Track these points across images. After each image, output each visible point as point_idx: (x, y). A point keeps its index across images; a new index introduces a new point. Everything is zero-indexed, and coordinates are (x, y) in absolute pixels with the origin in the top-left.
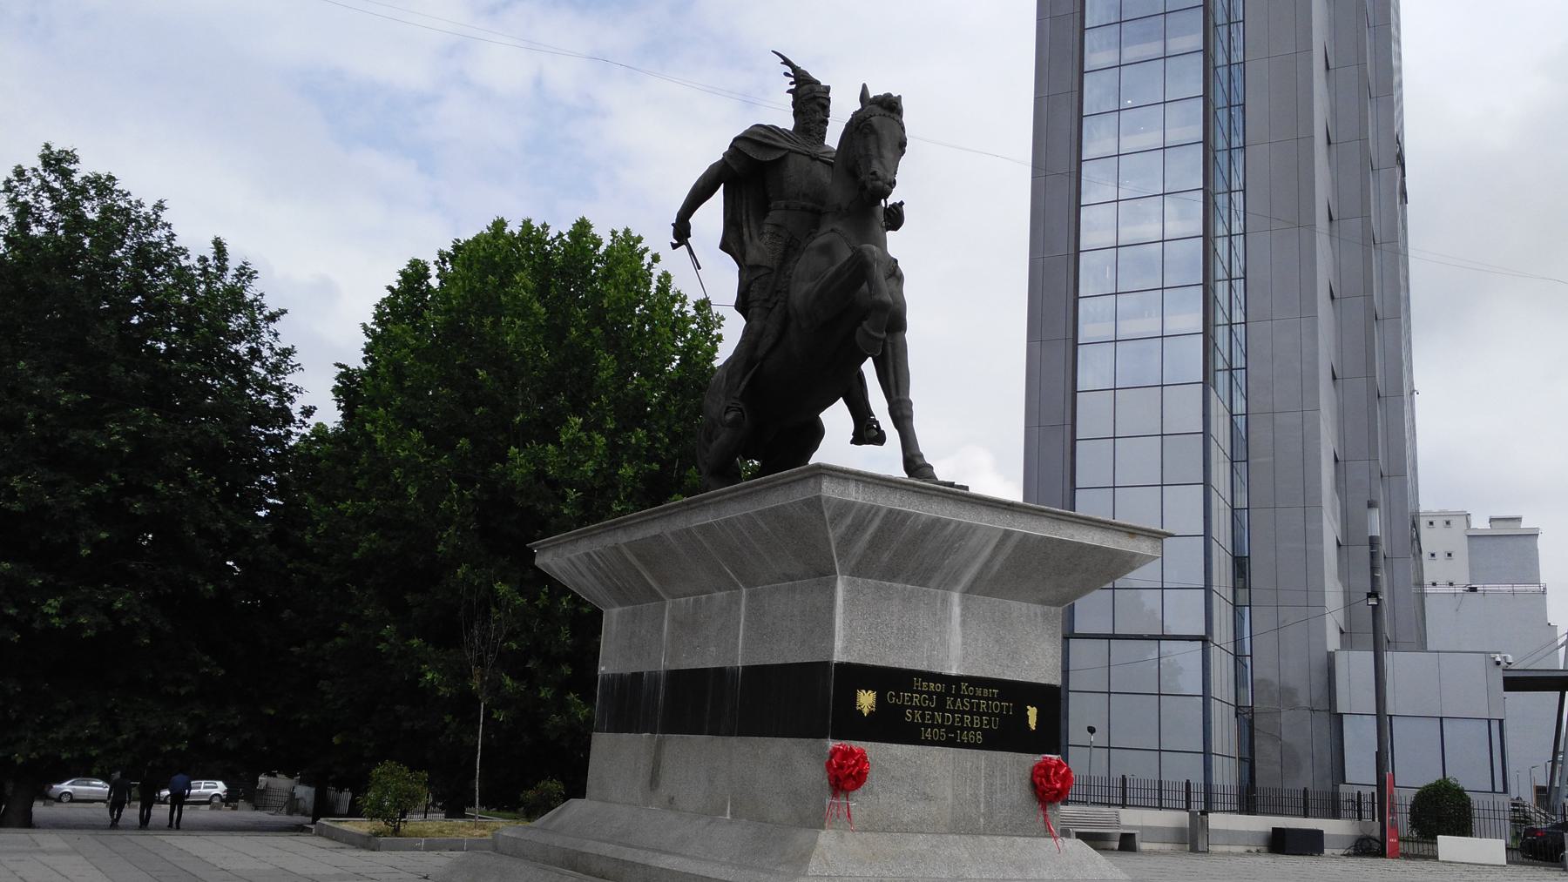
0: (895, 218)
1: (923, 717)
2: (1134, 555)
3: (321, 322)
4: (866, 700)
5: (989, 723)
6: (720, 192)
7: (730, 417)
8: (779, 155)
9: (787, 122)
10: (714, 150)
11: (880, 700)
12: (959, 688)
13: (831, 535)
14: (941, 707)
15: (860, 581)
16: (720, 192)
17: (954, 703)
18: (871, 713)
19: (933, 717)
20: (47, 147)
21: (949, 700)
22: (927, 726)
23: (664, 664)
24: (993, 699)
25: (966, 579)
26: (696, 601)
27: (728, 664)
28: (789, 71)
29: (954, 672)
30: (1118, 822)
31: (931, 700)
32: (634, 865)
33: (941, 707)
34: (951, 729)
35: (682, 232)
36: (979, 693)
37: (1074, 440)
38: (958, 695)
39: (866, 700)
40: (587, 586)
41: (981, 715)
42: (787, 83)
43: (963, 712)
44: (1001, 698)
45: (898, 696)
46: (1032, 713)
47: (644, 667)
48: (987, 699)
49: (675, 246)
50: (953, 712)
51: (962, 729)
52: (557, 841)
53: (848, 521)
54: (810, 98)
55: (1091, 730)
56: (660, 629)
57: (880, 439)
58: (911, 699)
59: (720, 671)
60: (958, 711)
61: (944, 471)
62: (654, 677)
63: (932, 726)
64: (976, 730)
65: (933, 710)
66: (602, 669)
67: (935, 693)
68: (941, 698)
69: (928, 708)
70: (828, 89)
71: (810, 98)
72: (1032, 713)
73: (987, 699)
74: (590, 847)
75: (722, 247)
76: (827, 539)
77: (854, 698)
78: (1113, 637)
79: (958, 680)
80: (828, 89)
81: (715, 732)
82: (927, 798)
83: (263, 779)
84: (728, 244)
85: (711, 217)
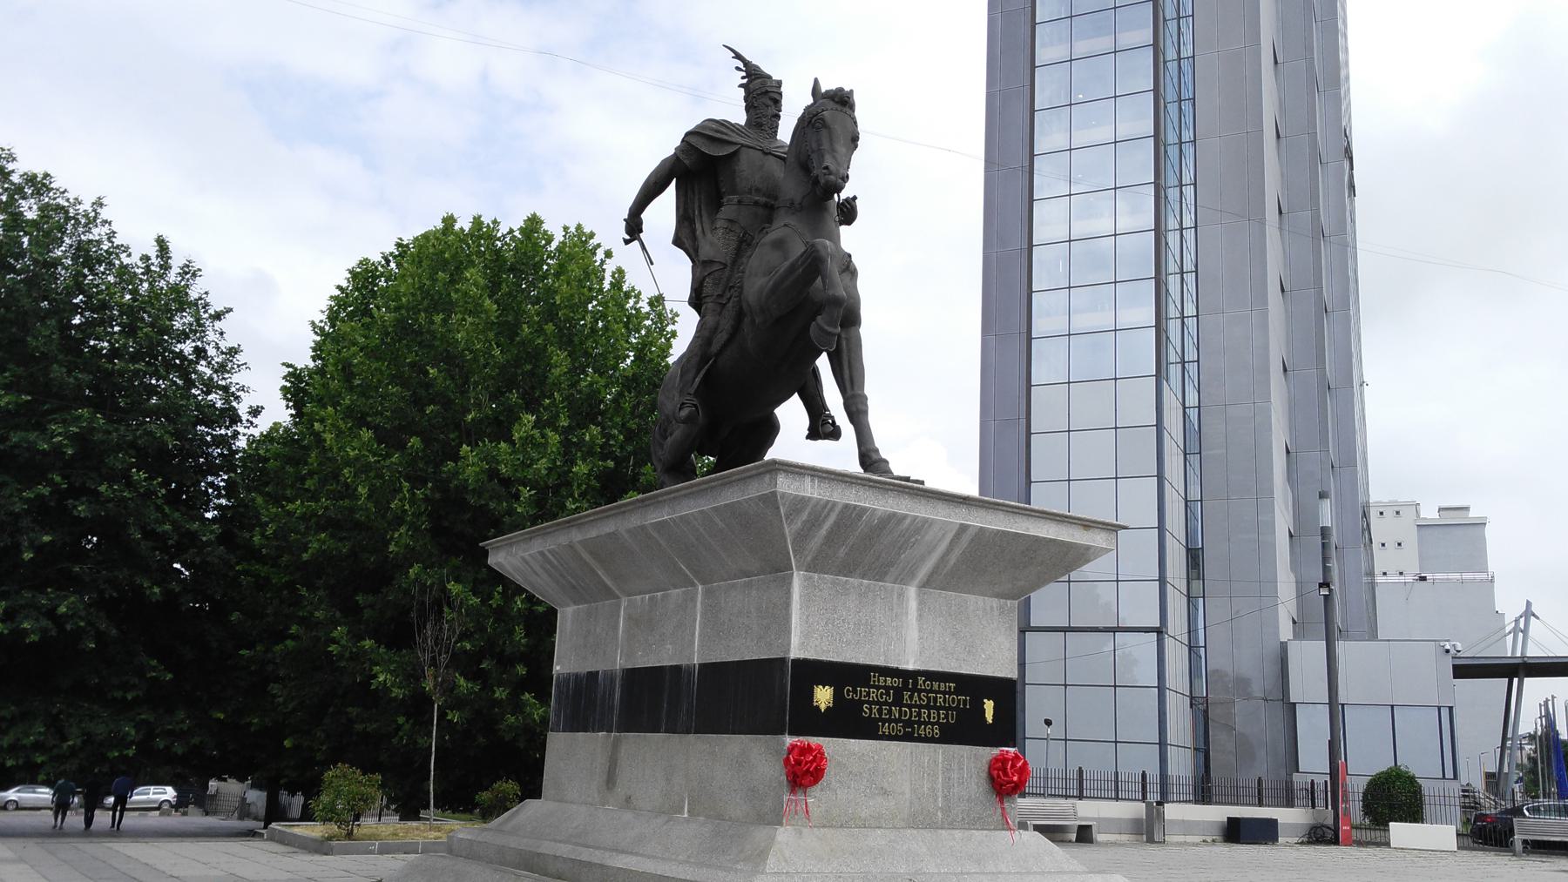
0: (848, 213)
2: (1088, 548)
3: (267, 327)
4: (823, 696)
5: (946, 717)
6: (672, 187)
7: (684, 413)
8: (731, 149)
9: (739, 116)
10: (666, 145)
11: (837, 696)
12: (915, 683)
14: (898, 702)
15: (816, 576)
17: (911, 697)
18: (828, 708)
19: (890, 712)
20: (855, 198)
21: (906, 695)
22: (884, 721)
23: (620, 663)
24: (950, 693)
25: (923, 573)
27: (683, 662)
28: (741, 65)
29: (911, 667)
31: (888, 694)
32: (590, 864)
33: (898, 702)
34: (909, 723)
35: (634, 228)
38: (915, 689)
39: (823, 696)
41: (938, 709)
42: (739, 78)
43: (920, 707)
44: (957, 692)
45: (855, 692)
46: (989, 706)
48: (944, 693)
49: (627, 242)
53: (804, 516)
54: (761, 93)
55: (1048, 722)
58: (868, 694)
59: (677, 669)
60: (915, 706)
61: (899, 467)
62: (610, 676)
63: (890, 721)
64: (933, 724)
66: (557, 668)
68: (899, 693)
69: (886, 703)
70: (779, 83)
71: (761, 93)
72: (989, 706)
73: (944, 693)
74: (547, 848)
75: (677, 242)
76: (783, 536)
78: (1065, 630)
79: (915, 674)
84: (685, 238)
85: (663, 213)
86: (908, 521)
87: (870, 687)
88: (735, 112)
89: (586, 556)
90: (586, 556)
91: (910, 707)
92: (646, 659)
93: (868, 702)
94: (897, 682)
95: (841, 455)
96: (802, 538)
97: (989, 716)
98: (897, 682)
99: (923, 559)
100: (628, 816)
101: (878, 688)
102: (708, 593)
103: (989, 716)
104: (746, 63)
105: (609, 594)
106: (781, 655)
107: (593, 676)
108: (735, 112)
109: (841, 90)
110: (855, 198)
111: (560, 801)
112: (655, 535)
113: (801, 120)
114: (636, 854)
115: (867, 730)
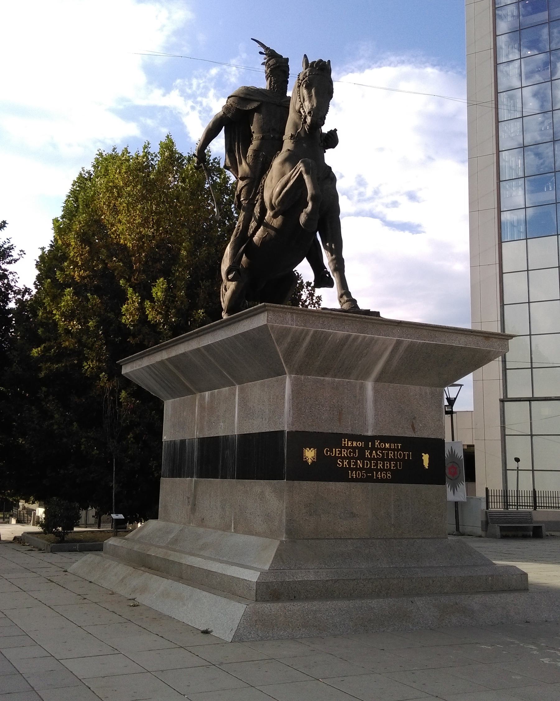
1: (349, 463)
2: (489, 352)
4: (310, 454)
5: (396, 465)
6: (222, 133)
9: (263, 84)
10: (217, 106)
11: (319, 454)
12: (373, 444)
13: (278, 350)
14: (362, 457)
15: (302, 377)
16: (222, 133)
17: (371, 454)
18: (313, 462)
19: (356, 463)
20: (336, 130)
22: (352, 470)
23: (197, 435)
24: (398, 450)
25: (375, 373)
26: (212, 394)
27: (229, 434)
28: (263, 50)
29: (370, 434)
30: (532, 519)
32: (173, 562)
33: (362, 457)
34: (370, 470)
36: (387, 445)
37: (501, 273)
38: (373, 448)
39: (310, 454)
40: (152, 386)
41: (390, 460)
42: (262, 59)
43: (377, 459)
44: (403, 449)
46: (426, 458)
47: (187, 437)
48: (394, 450)
50: (370, 460)
51: (377, 470)
52: (136, 547)
53: (289, 339)
55: (517, 460)
56: (193, 413)
57: (330, 284)
58: (341, 452)
59: (226, 438)
60: (374, 459)
61: (362, 305)
62: (192, 441)
63: (356, 469)
64: (386, 471)
65: (357, 459)
66: (165, 438)
67: (357, 447)
68: (362, 451)
69: (353, 458)
70: (287, 60)
71: (278, 67)
72: (426, 458)
73: (394, 450)
74: (152, 552)
76: (277, 352)
77: (302, 453)
78: (530, 400)
79: (372, 439)
80: (287, 60)
81: (224, 477)
82: (353, 515)
83: (22, 503)
86: (360, 339)
87: (342, 448)
88: (262, 82)
89: (171, 367)
90: (171, 367)
91: (370, 460)
92: (207, 434)
93: (341, 458)
94: (360, 444)
95: (329, 298)
96: (289, 354)
97: (426, 463)
98: (360, 444)
99: (375, 363)
100: (201, 530)
101: (348, 448)
102: (242, 391)
103: (426, 463)
104: (267, 49)
105: (192, 393)
106: (282, 429)
107: (183, 442)
108: (262, 82)
109: (321, 61)
110: (336, 130)
111: (167, 521)
112: (206, 353)
113: (332, 92)
114: (199, 556)
115: (341, 476)
